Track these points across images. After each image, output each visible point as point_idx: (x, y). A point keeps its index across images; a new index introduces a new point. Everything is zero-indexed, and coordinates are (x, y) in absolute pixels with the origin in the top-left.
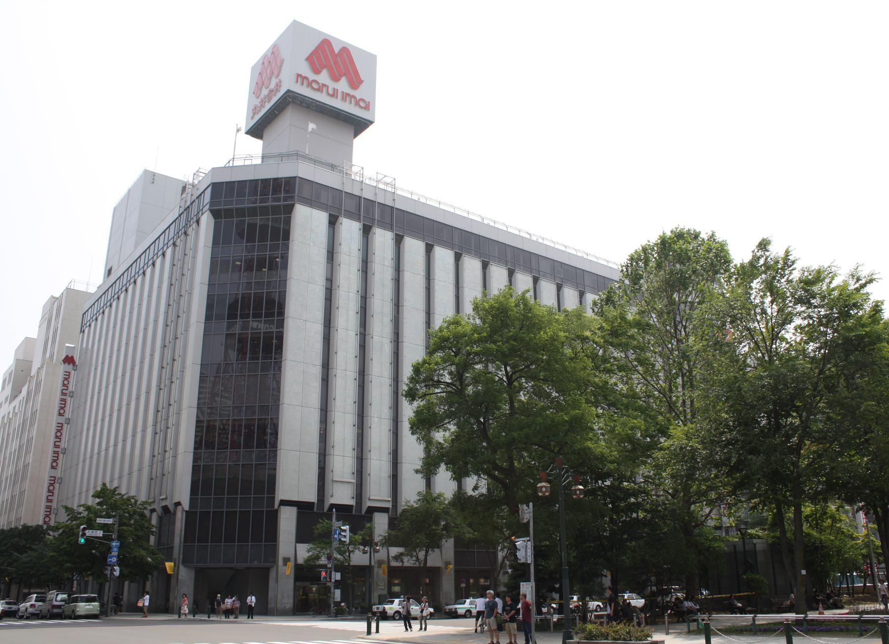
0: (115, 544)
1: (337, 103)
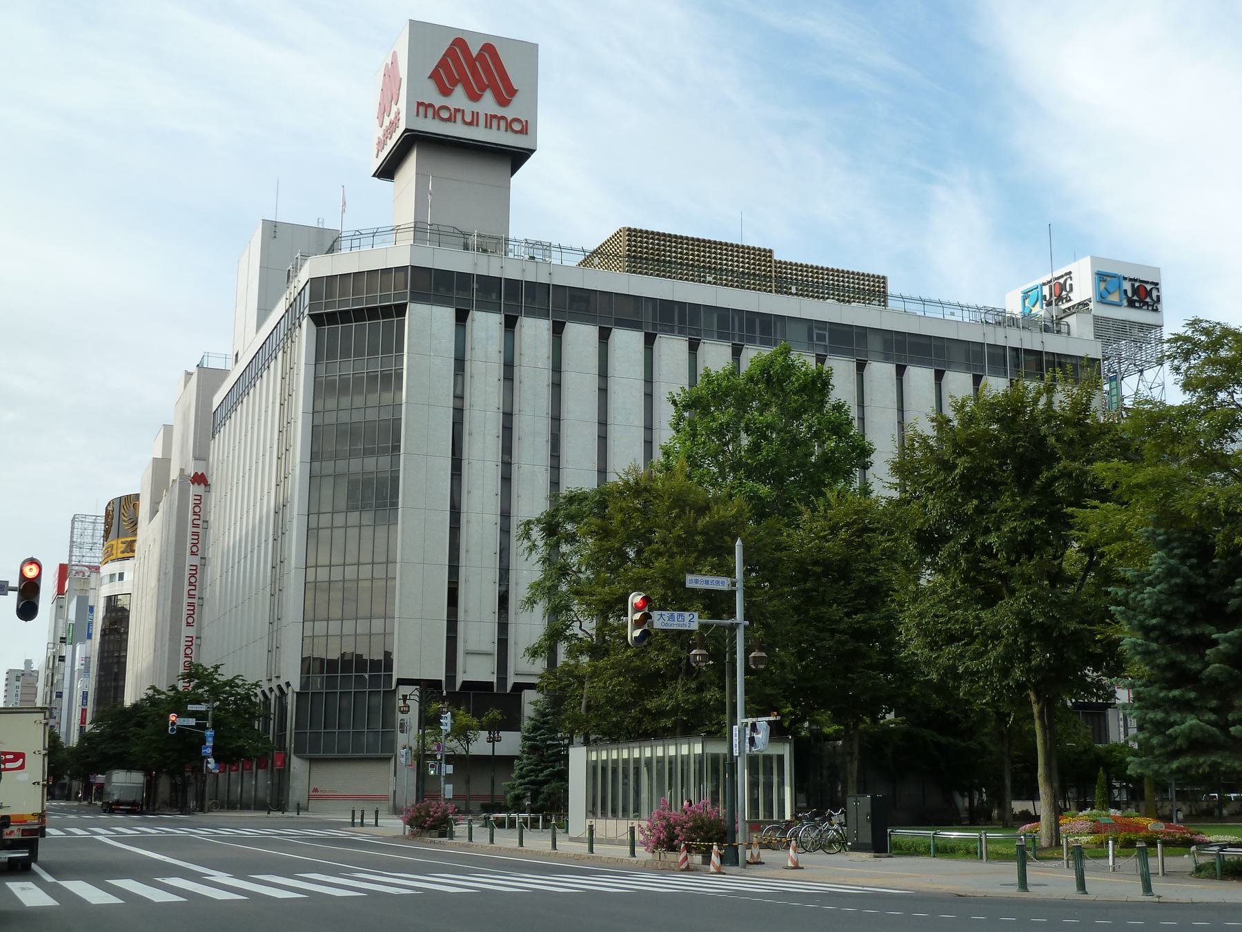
0: (209, 733)
1: (479, 134)
